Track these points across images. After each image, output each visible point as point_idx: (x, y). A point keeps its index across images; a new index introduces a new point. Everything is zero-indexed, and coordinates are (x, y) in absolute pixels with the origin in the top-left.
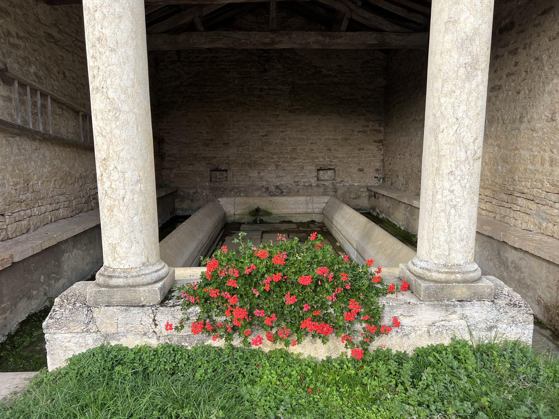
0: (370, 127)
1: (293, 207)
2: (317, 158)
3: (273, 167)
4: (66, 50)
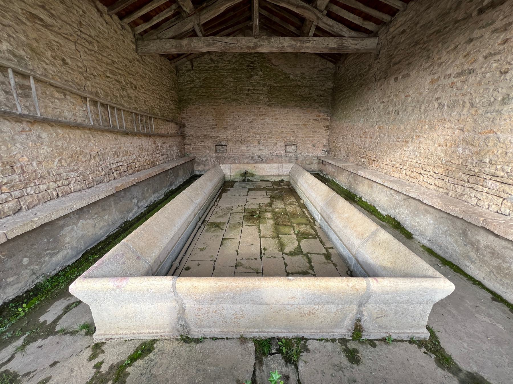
0: (321, 116)
1: (269, 170)
2: (285, 137)
3: (256, 144)
4: (64, 37)
